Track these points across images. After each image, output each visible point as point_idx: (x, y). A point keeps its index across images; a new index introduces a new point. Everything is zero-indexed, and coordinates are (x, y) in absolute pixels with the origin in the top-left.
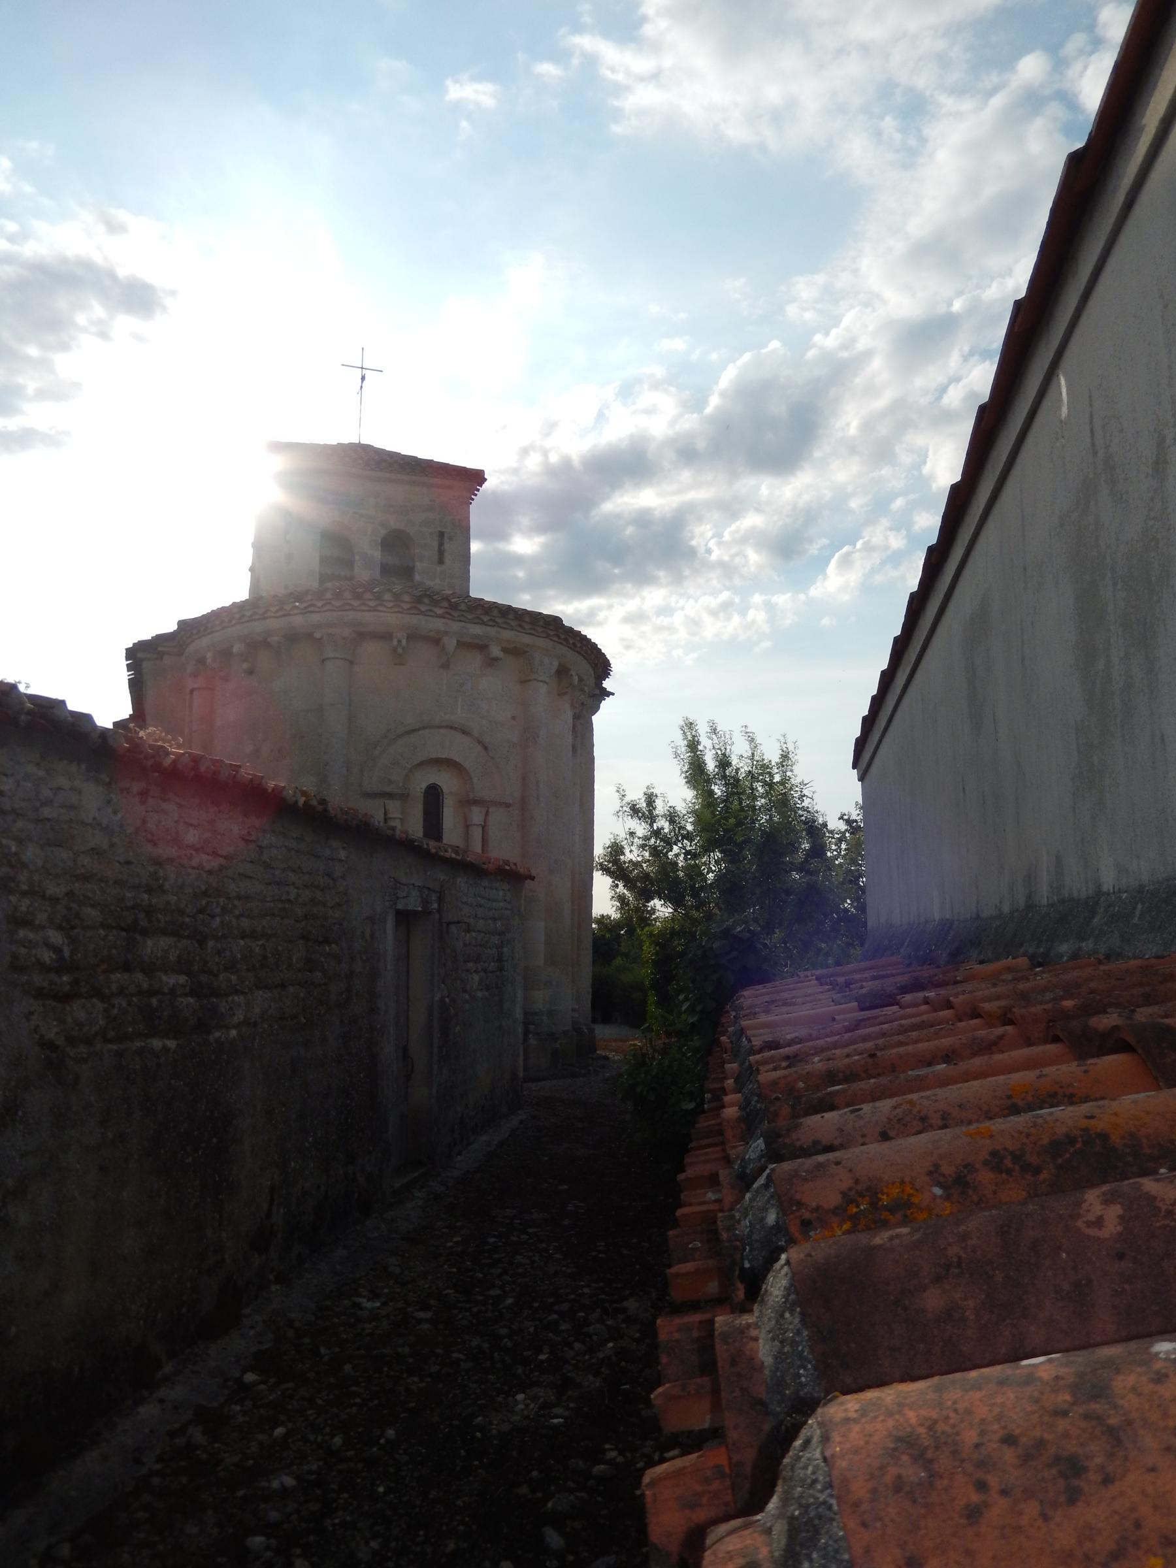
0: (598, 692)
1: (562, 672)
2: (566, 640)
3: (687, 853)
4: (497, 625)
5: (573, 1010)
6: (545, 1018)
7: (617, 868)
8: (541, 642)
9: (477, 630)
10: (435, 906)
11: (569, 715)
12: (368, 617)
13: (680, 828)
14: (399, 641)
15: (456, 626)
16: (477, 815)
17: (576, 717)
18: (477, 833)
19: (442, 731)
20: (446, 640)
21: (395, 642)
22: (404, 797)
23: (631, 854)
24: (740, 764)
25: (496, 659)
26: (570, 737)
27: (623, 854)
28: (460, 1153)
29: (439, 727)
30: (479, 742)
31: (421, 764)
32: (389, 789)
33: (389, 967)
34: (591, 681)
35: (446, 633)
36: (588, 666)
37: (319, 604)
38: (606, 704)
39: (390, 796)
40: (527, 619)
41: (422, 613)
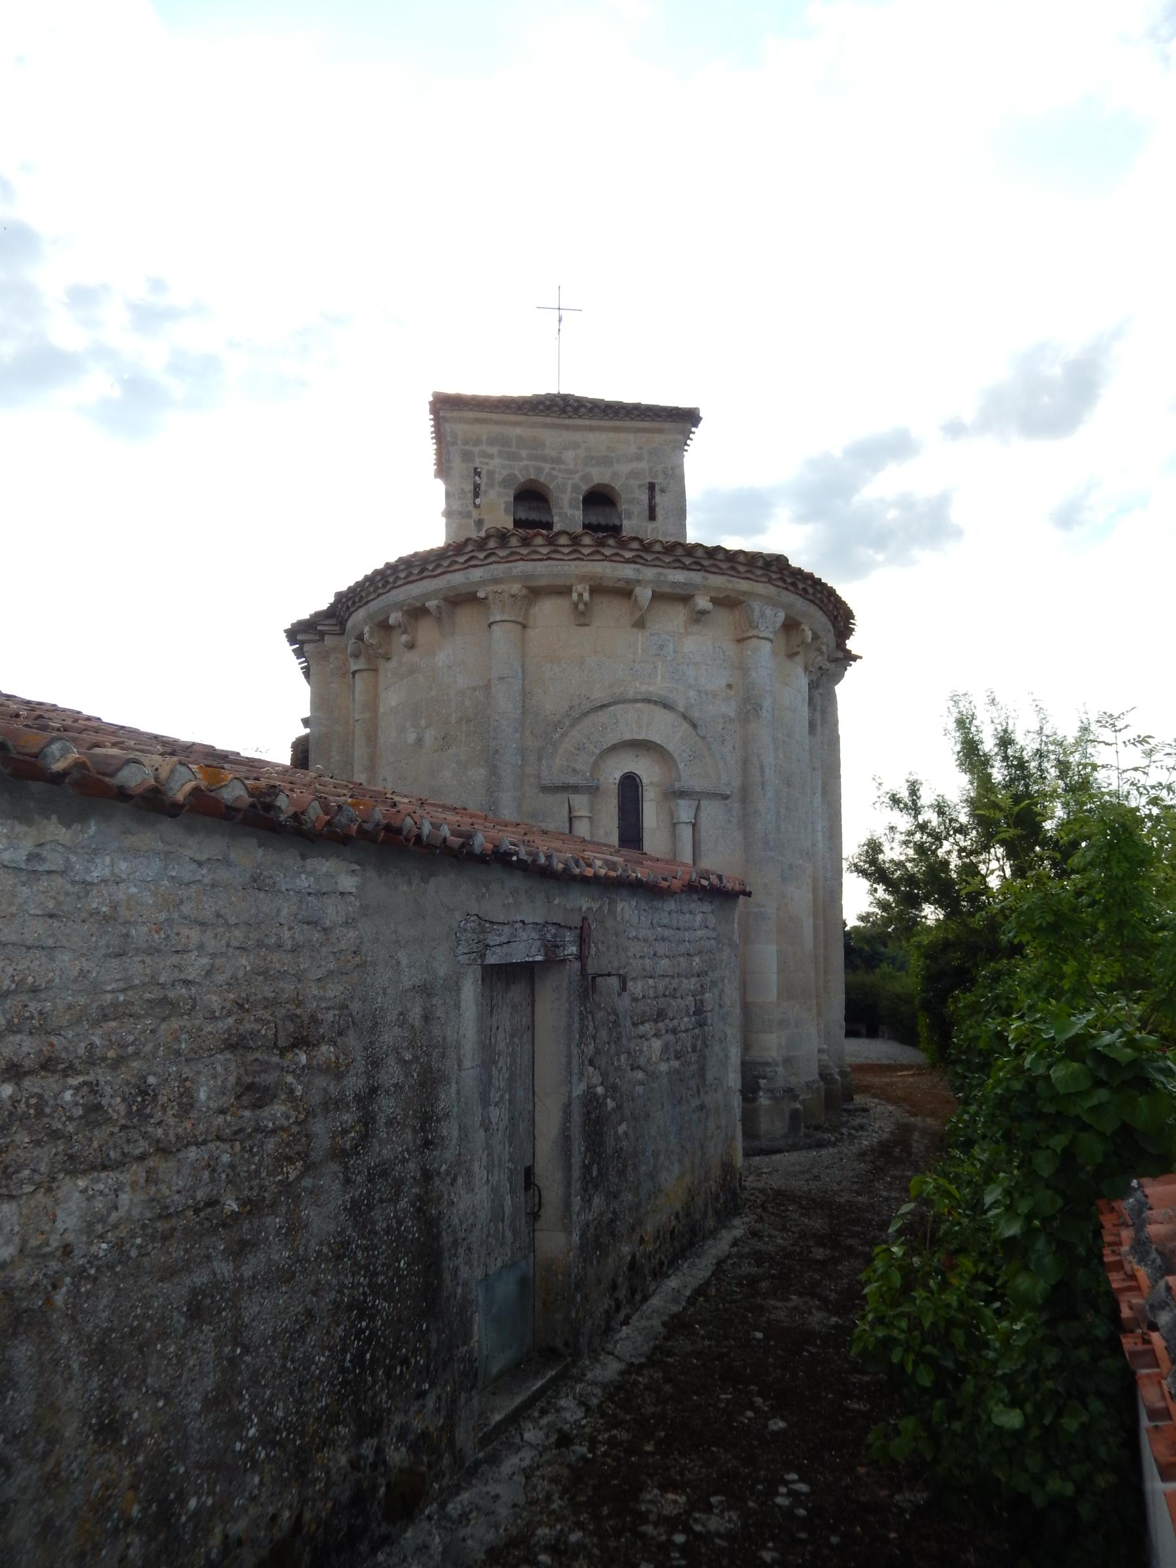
0: (841, 655)
1: (790, 626)
2: (793, 584)
3: (962, 850)
4: (703, 569)
5: (820, 1051)
6: (780, 1069)
7: (874, 868)
8: (761, 588)
9: (678, 576)
10: (573, 949)
11: (803, 682)
12: (540, 568)
13: (951, 820)
14: (580, 595)
15: (649, 573)
16: (685, 811)
17: (813, 686)
18: (686, 833)
19: (638, 705)
20: (638, 590)
21: (575, 596)
22: (593, 790)
23: (893, 852)
24: (1026, 743)
25: (703, 613)
26: (806, 708)
27: (881, 851)
28: (626, 1322)
29: (635, 701)
30: (685, 717)
31: (614, 748)
32: (572, 781)
33: (467, 1063)
34: (829, 638)
35: (638, 582)
36: (824, 619)
37: (481, 555)
38: (853, 672)
39: (575, 789)
40: (742, 559)
41: (607, 558)
